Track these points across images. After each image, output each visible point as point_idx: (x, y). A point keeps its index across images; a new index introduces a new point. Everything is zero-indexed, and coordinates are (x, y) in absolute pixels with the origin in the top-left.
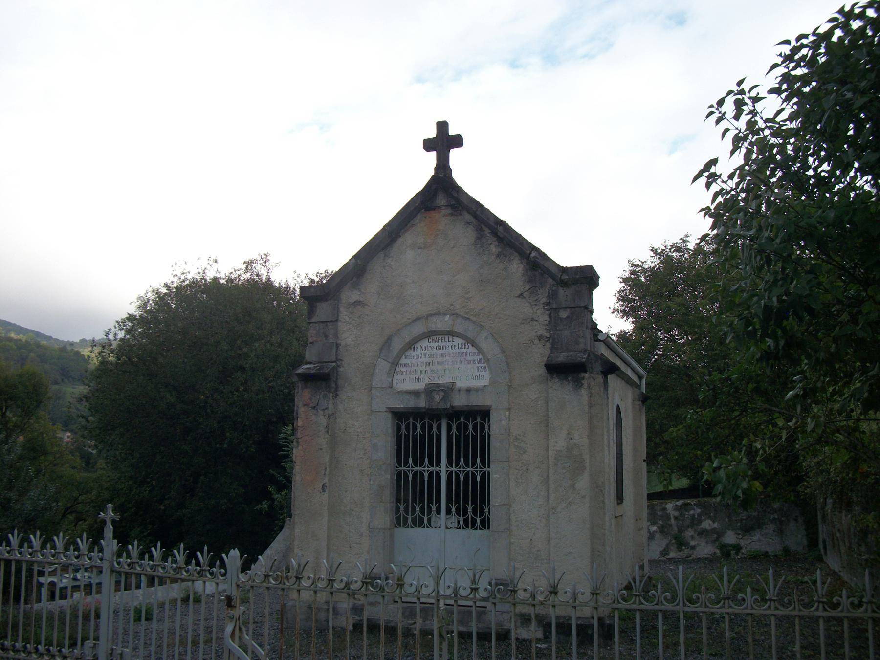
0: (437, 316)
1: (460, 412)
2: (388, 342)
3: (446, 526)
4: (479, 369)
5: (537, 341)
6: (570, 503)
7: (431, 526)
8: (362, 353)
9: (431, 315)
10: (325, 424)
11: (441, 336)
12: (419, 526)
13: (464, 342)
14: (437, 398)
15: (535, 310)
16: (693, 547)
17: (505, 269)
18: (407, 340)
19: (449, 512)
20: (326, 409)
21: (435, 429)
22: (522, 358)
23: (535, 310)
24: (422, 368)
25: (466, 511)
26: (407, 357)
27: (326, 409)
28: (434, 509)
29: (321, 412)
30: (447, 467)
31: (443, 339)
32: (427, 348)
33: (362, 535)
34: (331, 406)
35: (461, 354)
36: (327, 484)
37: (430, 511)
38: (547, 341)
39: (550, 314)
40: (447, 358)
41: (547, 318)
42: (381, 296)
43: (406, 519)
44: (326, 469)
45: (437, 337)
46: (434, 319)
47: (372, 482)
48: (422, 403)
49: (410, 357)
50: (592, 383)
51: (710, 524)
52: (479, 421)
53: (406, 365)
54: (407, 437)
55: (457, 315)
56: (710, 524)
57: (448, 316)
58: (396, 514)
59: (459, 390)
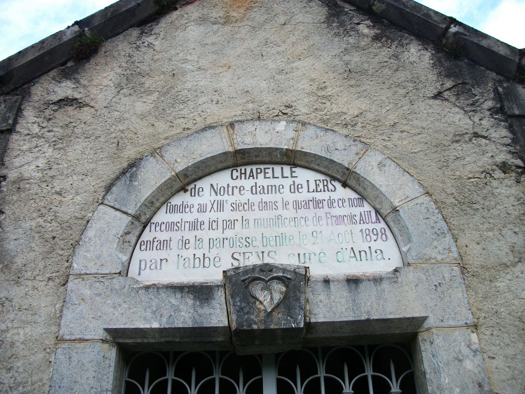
4: (366, 234)
5: (498, 174)
8: (55, 196)
11: (262, 167)
13: (321, 177)
15: (476, 119)
18: (180, 167)
22: (475, 206)
24: (213, 234)
26: (174, 209)
31: (270, 171)
32: (227, 190)
35: (318, 204)
40: (280, 211)
41: (504, 132)
42: (125, 90)
45: (254, 168)
46: (249, 127)
49: (183, 208)
53: (171, 226)
57: (283, 123)
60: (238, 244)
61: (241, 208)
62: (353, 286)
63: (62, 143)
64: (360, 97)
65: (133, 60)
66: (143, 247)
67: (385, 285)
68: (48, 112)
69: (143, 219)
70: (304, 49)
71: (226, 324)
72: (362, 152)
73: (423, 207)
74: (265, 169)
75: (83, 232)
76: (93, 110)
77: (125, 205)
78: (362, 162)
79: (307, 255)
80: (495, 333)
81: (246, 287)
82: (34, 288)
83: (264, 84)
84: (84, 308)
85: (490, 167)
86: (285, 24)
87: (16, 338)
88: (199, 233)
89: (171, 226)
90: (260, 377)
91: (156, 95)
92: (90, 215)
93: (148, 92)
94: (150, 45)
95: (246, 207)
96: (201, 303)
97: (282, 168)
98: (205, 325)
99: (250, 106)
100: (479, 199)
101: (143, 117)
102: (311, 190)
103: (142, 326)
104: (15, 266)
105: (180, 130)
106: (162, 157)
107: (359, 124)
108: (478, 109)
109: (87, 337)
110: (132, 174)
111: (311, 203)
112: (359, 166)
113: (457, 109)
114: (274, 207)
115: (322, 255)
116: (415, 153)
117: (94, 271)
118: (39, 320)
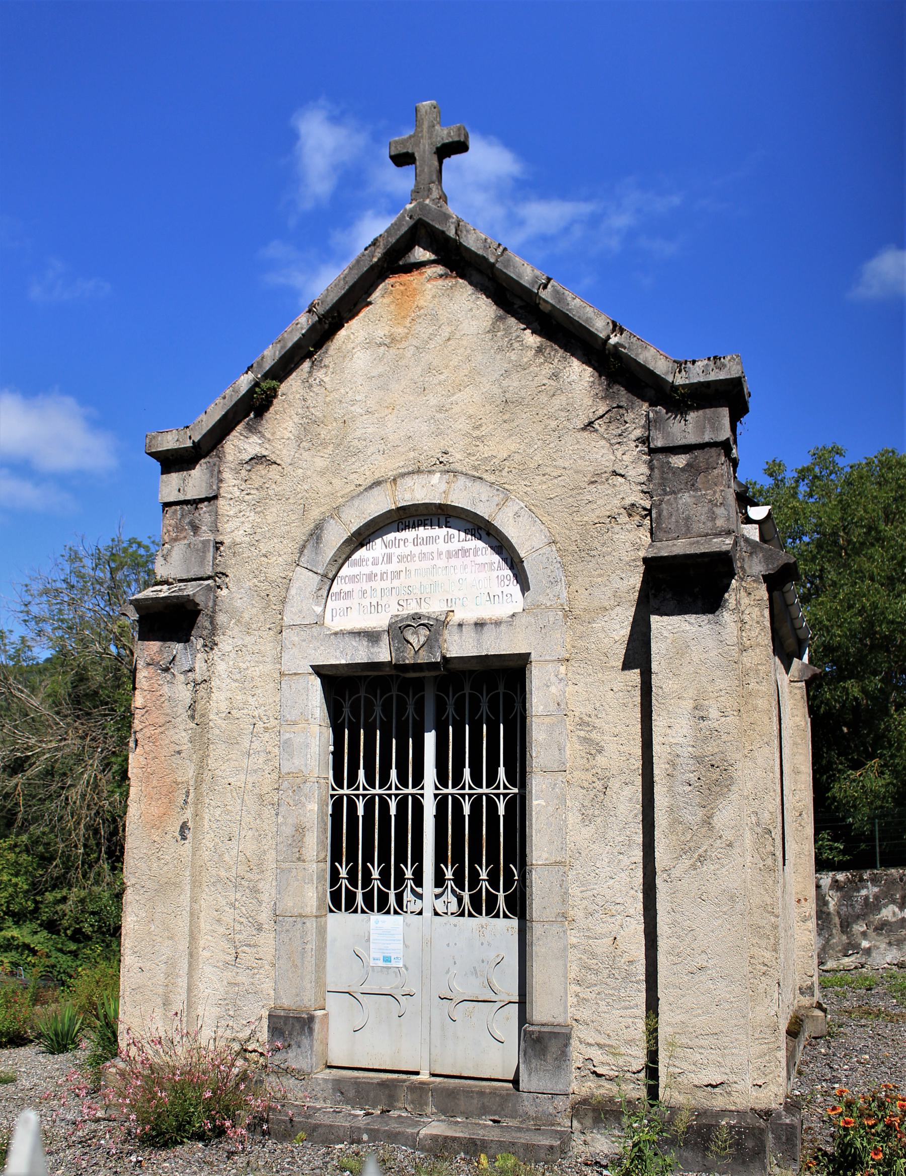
0: (415, 476)
1: (463, 672)
2: (316, 534)
3: (435, 910)
5: (624, 518)
6: (702, 859)
7: (402, 909)
8: (263, 559)
9: (403, 475)
10: (188, 702)
12: (378, 911)
14: (417, 639)
15: (619, 454)
16: (868, 952)
17: (555, 376)
19: (439, 880)
20: (190, 671)
21: (411, 710)
22: (592, 553)
23: (619, 454)
24: (386, 584)
25: (475, 879)
26: (355, 564)
27: (190, 671)
28: (409, 874)
29: (181, 678)
30: (437, 788)
33: (260, 929)
34: (200, 665)
36: (190, 824)
37: (400, 879)
38: (646, 515)
39: (651, 461)
41: (644, 469)
42: (304, 443)
43: (351, 897)
44: (188, 792)
46: (408, 481)
47: (280, 819)
48: (383, 654)
50: (745, 601)
51: (894, 913)
52: (501, 690)
53: (353, 579)
54: (368, 857)
55: (455, 472)
56: (894, 913)
57: (438, 475)
58: (333, 884)
59: (460, 625)
60: (403, 592)
61: (405, 559)
62: (479, 628)
63: (260, 506)
64: (511, 435)
65: (307, 404)
66: (334, 598)
67: (503, 627)
68: (244, 473)
69: (331, 576)
70: (465, 376)
71: (390, 660)
72: (502, 503)
73: (545, 557)
74: (425, 520)
75: (287, 589)
76: (280, 468)
77: (315, 566)
78: (500, 513)
79: (454, 600)
80: (581, 665)
81: (402, 632)
82: (261, 637)
83: (424, 428)
84: (295, 651)
85: (616, 510)
86: (449, 339)
87: (254, 673)
88: (373, 584)
89: (353, 579)
90: (422, 693)
91: (331, 447)
92: (291, 574)
93: (324, 444)
94: (321, 383)
95: (409, 558)
96: (373, 644)
97: (439, 519)
98: (376, 661)
99: (412, 454)
100: (598, 546)
101: (322, 473)
102: (461, 540)
103: (334, 663)
104: (244, 620)
105: (353, 487)
106: (339, 518)
107: (506, 469)
108: (625, 440)
109: (299, 672)
110: (318, 537)
111: (460, 552)
112: (498, 518)
113: (603, 442)
114: (431, 557)
115: (465, 599)
116: (551, 499)
117: (299, 623)
118: (267, 660)
